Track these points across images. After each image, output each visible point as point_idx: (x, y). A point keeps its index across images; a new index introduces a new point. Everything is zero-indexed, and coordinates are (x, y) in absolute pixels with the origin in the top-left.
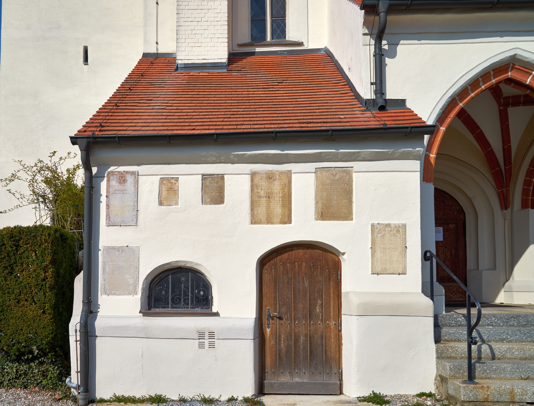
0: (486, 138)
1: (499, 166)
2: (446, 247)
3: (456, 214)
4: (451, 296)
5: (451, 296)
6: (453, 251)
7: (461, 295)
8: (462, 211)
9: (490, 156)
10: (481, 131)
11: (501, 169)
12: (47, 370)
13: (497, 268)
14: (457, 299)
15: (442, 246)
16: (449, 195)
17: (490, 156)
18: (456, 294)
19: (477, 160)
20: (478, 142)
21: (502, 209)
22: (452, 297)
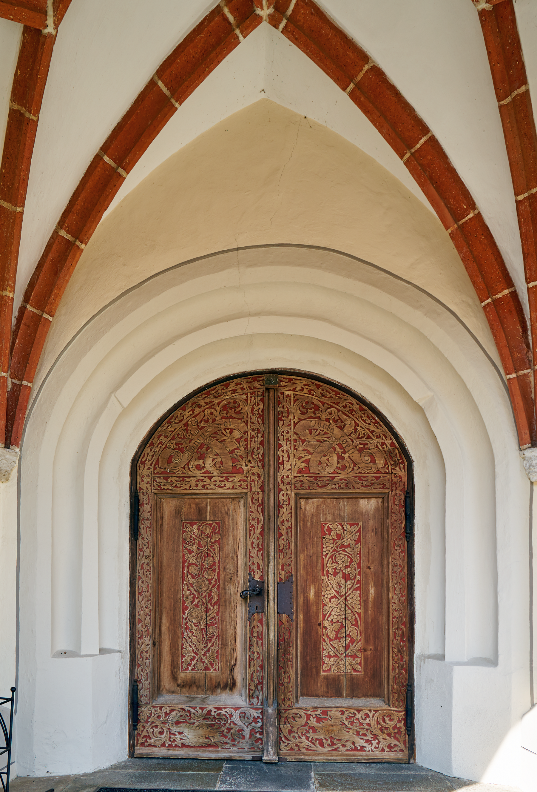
0: (452, 171)
1: (509, 282)
2: (346, 577)
3: (380, 463)
4: (360, 742)
5: (360, 742)
6: (372, 591)
7: (394, 742)
8: (401, 455)
9: (472, 239)
10: (433, 142)
11: (514, 295)
12: (391, 720)
13: (501, 658)
14: (378, 754)
15: (335, 574)
16: (361, 400)
17: (472, 239)
18: (375, 737)
19: (438, 269)
20: (422, 185)
21: (521, 443)
22: (362, 749)
